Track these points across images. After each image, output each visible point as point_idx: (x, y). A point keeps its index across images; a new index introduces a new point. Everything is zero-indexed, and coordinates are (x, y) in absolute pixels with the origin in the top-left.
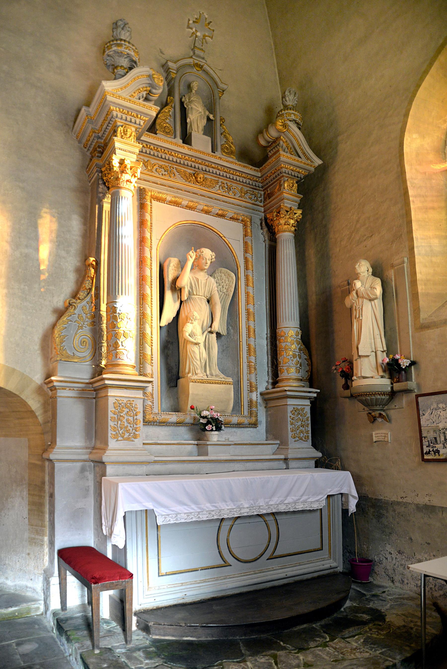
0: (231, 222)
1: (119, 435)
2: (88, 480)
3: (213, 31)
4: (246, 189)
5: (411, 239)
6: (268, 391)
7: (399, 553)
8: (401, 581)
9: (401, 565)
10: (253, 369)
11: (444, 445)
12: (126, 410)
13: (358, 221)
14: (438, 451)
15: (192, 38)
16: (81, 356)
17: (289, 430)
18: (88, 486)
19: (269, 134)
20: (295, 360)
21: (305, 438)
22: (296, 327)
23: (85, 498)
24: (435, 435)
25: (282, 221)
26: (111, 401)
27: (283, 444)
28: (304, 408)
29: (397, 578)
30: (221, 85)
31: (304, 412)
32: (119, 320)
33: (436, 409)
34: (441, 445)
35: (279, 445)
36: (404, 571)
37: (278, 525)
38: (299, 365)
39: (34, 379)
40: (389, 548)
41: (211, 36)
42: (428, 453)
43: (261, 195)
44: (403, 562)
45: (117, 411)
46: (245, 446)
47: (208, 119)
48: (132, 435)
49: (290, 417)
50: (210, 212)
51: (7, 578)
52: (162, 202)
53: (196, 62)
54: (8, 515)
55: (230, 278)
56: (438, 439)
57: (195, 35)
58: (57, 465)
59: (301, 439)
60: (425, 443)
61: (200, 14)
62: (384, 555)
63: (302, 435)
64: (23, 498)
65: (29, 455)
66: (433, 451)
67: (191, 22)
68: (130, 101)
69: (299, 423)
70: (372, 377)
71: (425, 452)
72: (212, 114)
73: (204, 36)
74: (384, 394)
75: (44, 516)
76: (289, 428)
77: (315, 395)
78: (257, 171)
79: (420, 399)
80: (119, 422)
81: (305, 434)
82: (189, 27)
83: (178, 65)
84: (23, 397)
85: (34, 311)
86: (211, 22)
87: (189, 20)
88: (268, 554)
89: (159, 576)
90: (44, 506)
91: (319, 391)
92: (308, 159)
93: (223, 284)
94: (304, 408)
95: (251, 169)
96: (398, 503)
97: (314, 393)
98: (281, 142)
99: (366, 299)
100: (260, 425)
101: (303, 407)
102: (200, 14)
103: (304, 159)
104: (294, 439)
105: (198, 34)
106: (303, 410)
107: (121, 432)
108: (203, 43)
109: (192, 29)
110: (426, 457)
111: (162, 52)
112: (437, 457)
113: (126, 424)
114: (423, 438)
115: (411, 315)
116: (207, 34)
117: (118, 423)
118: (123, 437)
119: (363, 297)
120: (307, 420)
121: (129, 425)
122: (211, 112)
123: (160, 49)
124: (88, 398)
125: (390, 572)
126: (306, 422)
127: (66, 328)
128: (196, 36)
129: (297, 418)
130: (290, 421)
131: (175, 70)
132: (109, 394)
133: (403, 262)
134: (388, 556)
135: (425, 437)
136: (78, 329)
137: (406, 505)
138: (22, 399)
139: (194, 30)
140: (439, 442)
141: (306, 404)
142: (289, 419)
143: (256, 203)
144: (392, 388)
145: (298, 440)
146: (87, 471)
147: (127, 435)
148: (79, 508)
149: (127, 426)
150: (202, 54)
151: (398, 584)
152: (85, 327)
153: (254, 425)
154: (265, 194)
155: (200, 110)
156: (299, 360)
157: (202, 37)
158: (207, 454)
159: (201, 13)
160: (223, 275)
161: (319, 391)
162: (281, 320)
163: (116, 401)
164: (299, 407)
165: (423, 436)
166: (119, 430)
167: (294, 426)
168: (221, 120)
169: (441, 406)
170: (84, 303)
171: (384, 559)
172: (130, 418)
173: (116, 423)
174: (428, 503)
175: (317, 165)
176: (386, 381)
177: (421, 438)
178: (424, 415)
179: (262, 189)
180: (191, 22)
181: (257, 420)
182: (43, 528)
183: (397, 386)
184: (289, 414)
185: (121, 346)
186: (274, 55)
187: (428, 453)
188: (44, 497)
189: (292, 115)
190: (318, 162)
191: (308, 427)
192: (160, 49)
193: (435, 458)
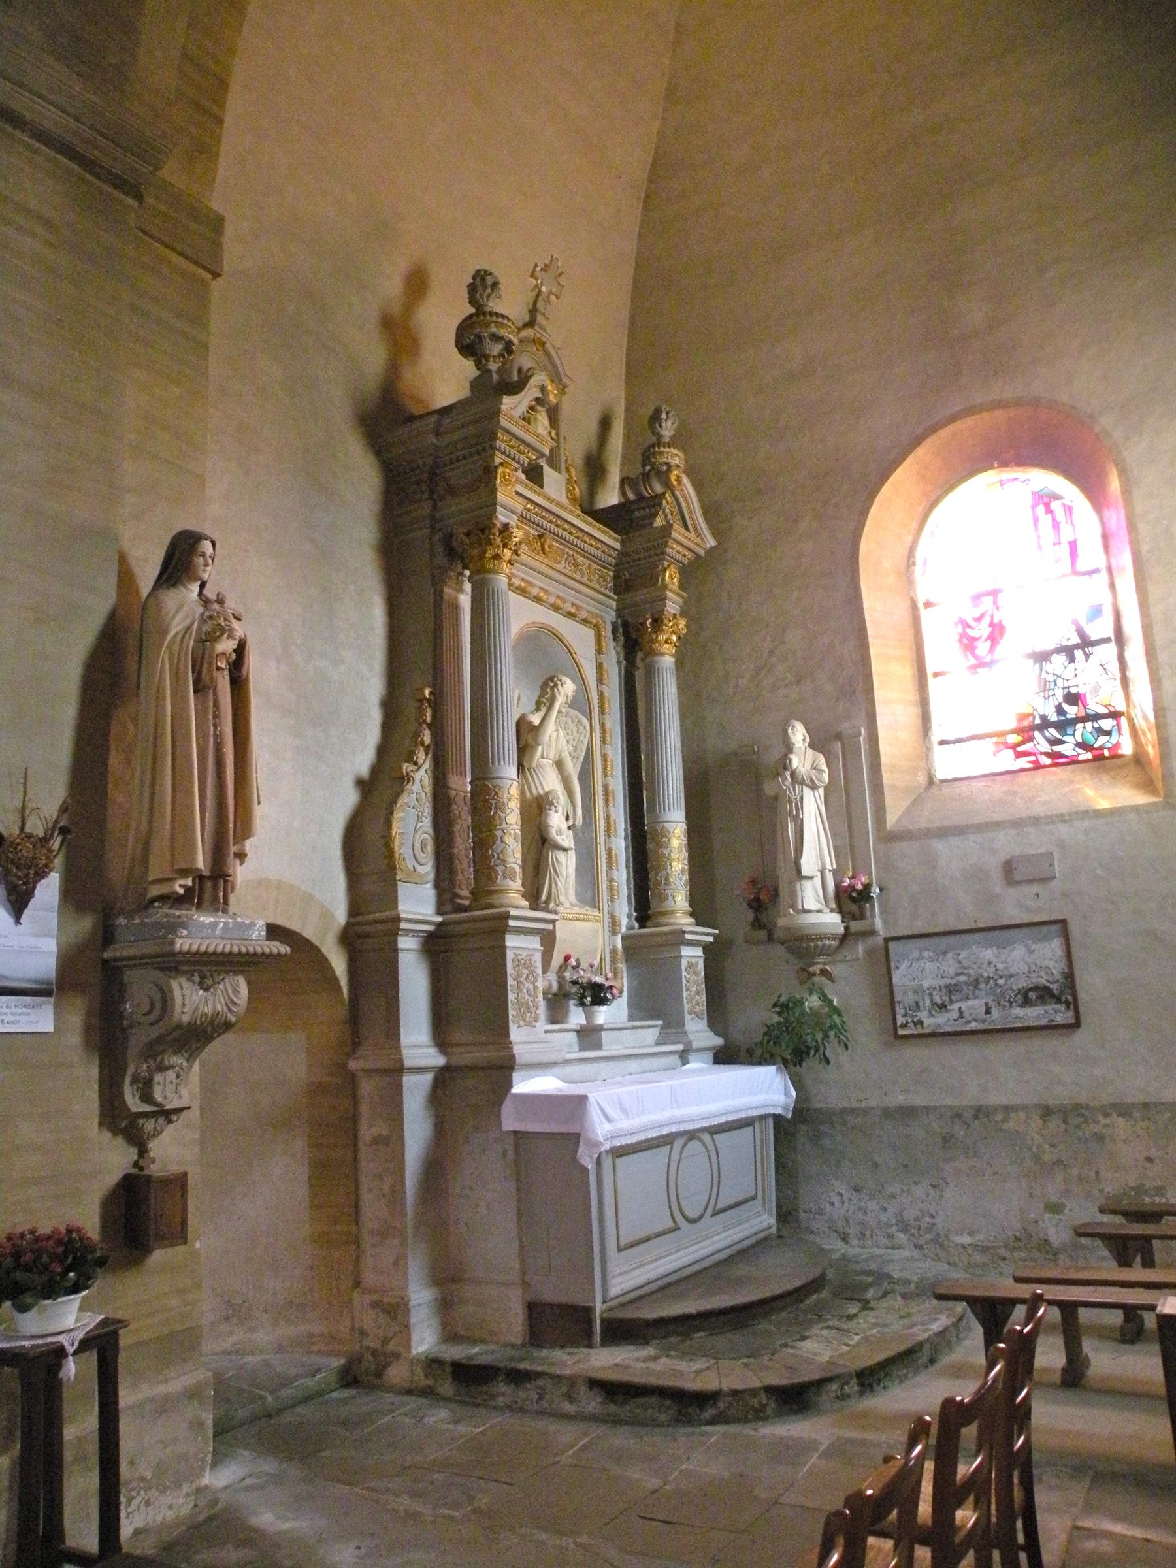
4: (595, 566)
5: (871, 702)
6: (632, 932)
7: (855, 1190)
8: (860, 1235)
9: (860, 1209)
11: (930, 1011)
14: (921, 1023)
24: (916, 998)
25: (662, 637)
26: (510, 955)
29: (853, 1231)
30: (565, 380)
32: (508, 811)
33: (918, 960)
34: (926, 1013)
36: (865, 1217)
40: (840, 1186)
42: (904, 1026)
44: (862, 1204)
50: (561, 609)
51: (252, 1330)
55: (582, 728)
56: (921, 1004)
60: (900, 1011)
62: (828, 1199)
66: (913, 1022)
67: (538, 269)
70: (818, 911)
71: (899, 1024)
73: (551, 293)
74: (834, 937)
77: (711, 939)
78: (617, 540)
79: (892, 945)
82: (532, 275)
88: (709, 1211)
91: (717, 932)
92: (699, 536)
95: (599, 529)
96: (852, 1111)
98: (664, 502)
99: (807, 786)
103: (692, 535)
105: (544, 289)
110: (901, 1032)
112: (919, 1031)
114: (897, 1004)
115: (871, 816)
119: (802, 783)
125: (840, 1224)
133: (860, 734)
134: (836, 1199)
135: (899, 1002)
137: (866, 1112)
140: (922, 1008)
142: (684, 981)
144: (847, 928)
151: (855, 1242)
158: (599, 1046)
160: (569, 720)
161: (717, 932)
162: (660, 809)
165: (896, 1000)
169: (926, 954)
171: (828, 1205)
174: (905, 1104)
175: (708, 546)
176: (835, 918)
177: (893, 1003)
178: (898, 968)
180: (538, 269)
183: (856, 926)
187: (904, 1026)
190: (711, 542)
193: (915, 1032)
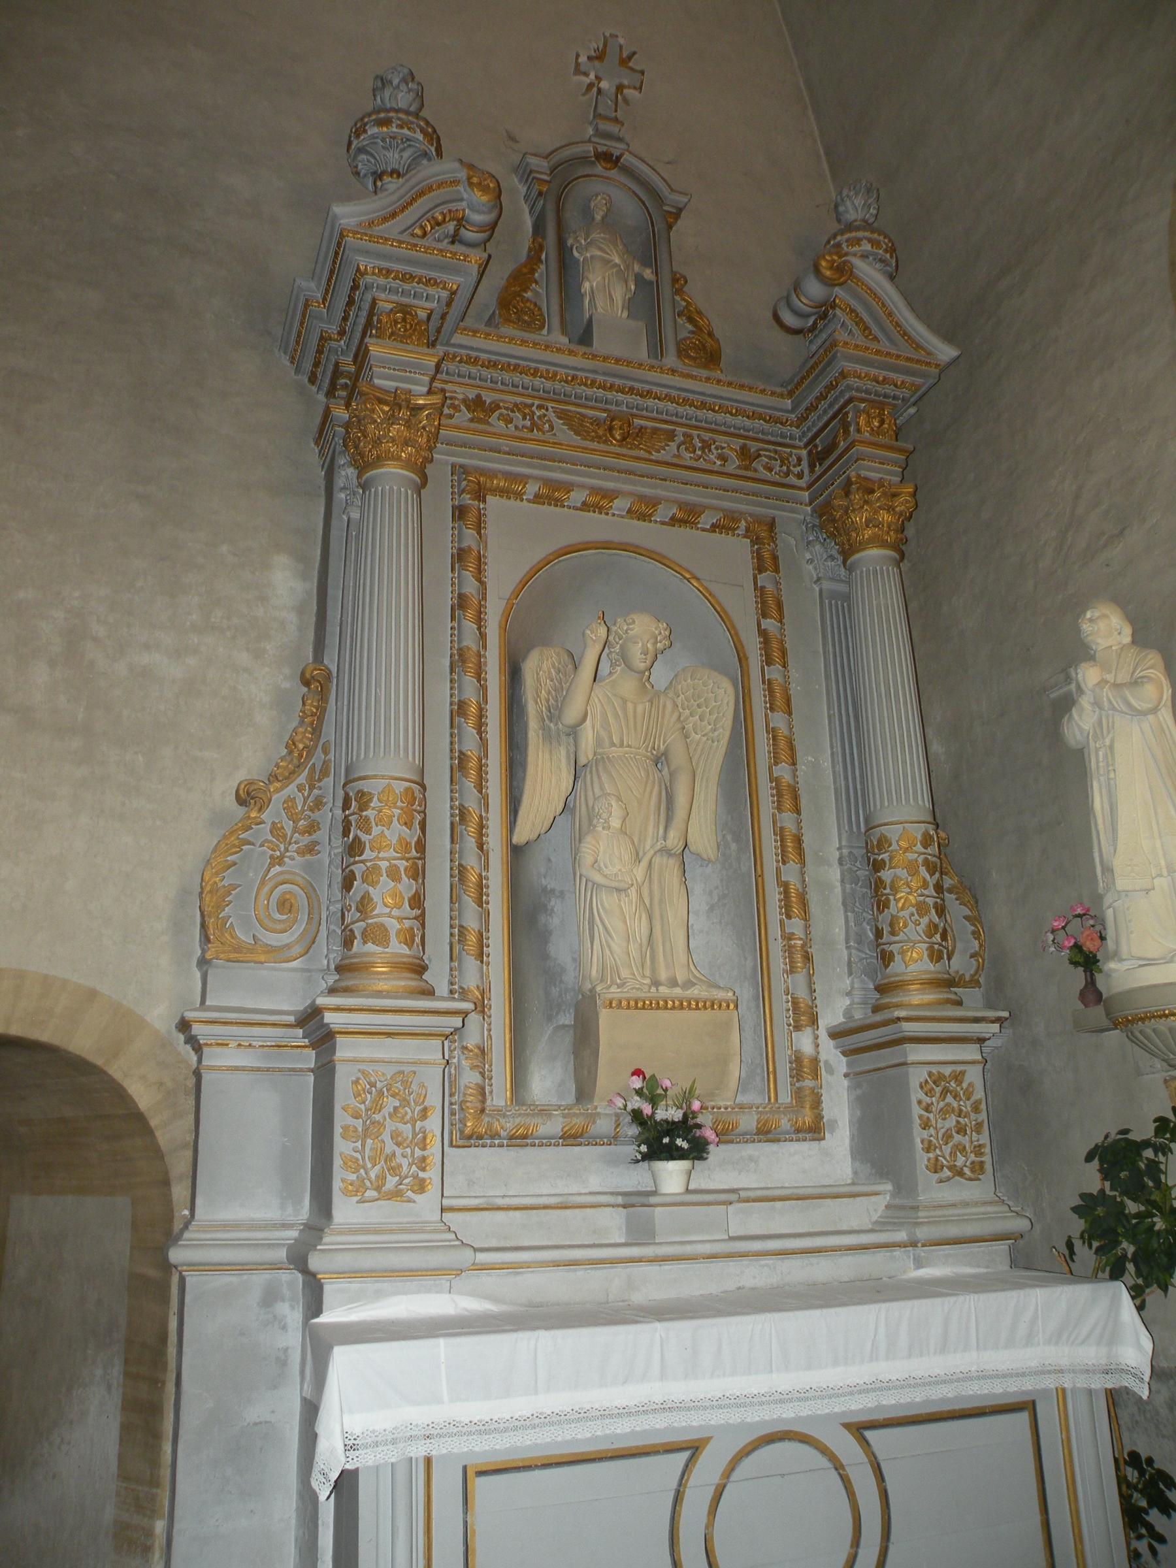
0: (676, 528)
1: (368, 1184)
2: (284, 1328)
3: (642, 73)
10: (798, 957)
12: (390, 1103)
13: (1077, 497)
15: (587, 97)
16: (275, 944)
17: (919, 1145)
18: (286, 1350)
19: (806, 297)
20: (925, 921)
21: (973, 1171)
22: (923, 819)
23: (275, 1387)
25: (859, 519)
27: (904, 1186)
28: (963, 1073)
31: (965, 1085)
35: (893, 1196)
37: (883, 1480)
38: (938, 936)
39: (148, 1018)
41: (638, 85)
43: (799, 459)
45: (362, 1107)
46: (779, 1204)
47: (639, 279)
48: (406, 1181)
49: (920, 1102)
52: (645, 521)
53: (601, 149)
54: (69, 1443)
57: (595, 90)
58: (192, 1280)
59: (960, 1173)
61: (605, 37)
63: (960, 1160)
64: (109, 1387)
65: (132, 1247)
67: (583, 59)
68: (896, 386)
69: (951, 1121)
72: (650, 266)
73: (620, 88)
75: (160, 1447)
76: (918, 1141)
80: (369, 1141)
81: (972, 1157)
82: (578, 70)
83: (552, 162)
84: (115, 1071)
85: (158, 823)
86: (634, 53)
87: (578, 56)
89: (1034, 1402)
90: (162, 1414)
93: (700, 710)
94: (963, 1073)
97: (993, 1022)
100: (832, 1132)
101: (959, 1068)
102: (605, 37)
104: (937, 1176)
105: (604, 85)
106: (958, 1077)
107: (373, 1175)
108: (616, 105)
109: (586, 74)
111: (512, 138)
113: (390, 1147)
116: (626, 82)
117: (363, 1146)
118: (378, 1189)
120: (976, 1109)
121: (398, 1151)
122: (645, 263)
123: (507, 131)
124: (294, 1070)
126: (973, 1116)
127: (235, 864)
128: (599, 91)
129: (942, 1104)
130: (920, 1117)
131: (545, 174)
132: (336, 1058)
136: (271, 865)
138: (113, 1080)
139: (592, 76)
141: (969, 1057)
142: (917, 1111)
143: (787, 480)
145: (949, 1179)
146: (283, 1300)
147: (391, 1182)
148: (256, 1424)
149: (394, 1154)
150: (614, 129)
152: (292, 859)
153: (815, 1130)
154: (810, 453)
155: (617, 260)
156: (936, 919)
157: (614, 90)
159: (607, 34)
163: (360, 1075)
164: (947, 1071)
166: (369, 1165)
167: (932, 1131)
168: (675, 280)
170: (291, 789)
172: (401, 1127)
173: (359, 1144)
179: (802, 444)
181: (819, 1117)
182: (154, 1490)
184: (917, 1094)
185: (380, 904)
186: (810, 112)
188: (164, 1383)
189: (865, 241)
191: (978, 1133)
192: (507, 131)
